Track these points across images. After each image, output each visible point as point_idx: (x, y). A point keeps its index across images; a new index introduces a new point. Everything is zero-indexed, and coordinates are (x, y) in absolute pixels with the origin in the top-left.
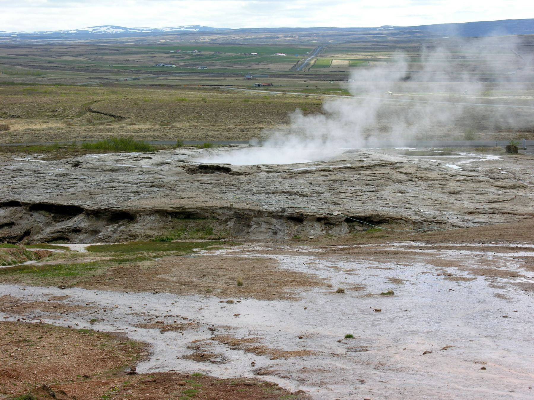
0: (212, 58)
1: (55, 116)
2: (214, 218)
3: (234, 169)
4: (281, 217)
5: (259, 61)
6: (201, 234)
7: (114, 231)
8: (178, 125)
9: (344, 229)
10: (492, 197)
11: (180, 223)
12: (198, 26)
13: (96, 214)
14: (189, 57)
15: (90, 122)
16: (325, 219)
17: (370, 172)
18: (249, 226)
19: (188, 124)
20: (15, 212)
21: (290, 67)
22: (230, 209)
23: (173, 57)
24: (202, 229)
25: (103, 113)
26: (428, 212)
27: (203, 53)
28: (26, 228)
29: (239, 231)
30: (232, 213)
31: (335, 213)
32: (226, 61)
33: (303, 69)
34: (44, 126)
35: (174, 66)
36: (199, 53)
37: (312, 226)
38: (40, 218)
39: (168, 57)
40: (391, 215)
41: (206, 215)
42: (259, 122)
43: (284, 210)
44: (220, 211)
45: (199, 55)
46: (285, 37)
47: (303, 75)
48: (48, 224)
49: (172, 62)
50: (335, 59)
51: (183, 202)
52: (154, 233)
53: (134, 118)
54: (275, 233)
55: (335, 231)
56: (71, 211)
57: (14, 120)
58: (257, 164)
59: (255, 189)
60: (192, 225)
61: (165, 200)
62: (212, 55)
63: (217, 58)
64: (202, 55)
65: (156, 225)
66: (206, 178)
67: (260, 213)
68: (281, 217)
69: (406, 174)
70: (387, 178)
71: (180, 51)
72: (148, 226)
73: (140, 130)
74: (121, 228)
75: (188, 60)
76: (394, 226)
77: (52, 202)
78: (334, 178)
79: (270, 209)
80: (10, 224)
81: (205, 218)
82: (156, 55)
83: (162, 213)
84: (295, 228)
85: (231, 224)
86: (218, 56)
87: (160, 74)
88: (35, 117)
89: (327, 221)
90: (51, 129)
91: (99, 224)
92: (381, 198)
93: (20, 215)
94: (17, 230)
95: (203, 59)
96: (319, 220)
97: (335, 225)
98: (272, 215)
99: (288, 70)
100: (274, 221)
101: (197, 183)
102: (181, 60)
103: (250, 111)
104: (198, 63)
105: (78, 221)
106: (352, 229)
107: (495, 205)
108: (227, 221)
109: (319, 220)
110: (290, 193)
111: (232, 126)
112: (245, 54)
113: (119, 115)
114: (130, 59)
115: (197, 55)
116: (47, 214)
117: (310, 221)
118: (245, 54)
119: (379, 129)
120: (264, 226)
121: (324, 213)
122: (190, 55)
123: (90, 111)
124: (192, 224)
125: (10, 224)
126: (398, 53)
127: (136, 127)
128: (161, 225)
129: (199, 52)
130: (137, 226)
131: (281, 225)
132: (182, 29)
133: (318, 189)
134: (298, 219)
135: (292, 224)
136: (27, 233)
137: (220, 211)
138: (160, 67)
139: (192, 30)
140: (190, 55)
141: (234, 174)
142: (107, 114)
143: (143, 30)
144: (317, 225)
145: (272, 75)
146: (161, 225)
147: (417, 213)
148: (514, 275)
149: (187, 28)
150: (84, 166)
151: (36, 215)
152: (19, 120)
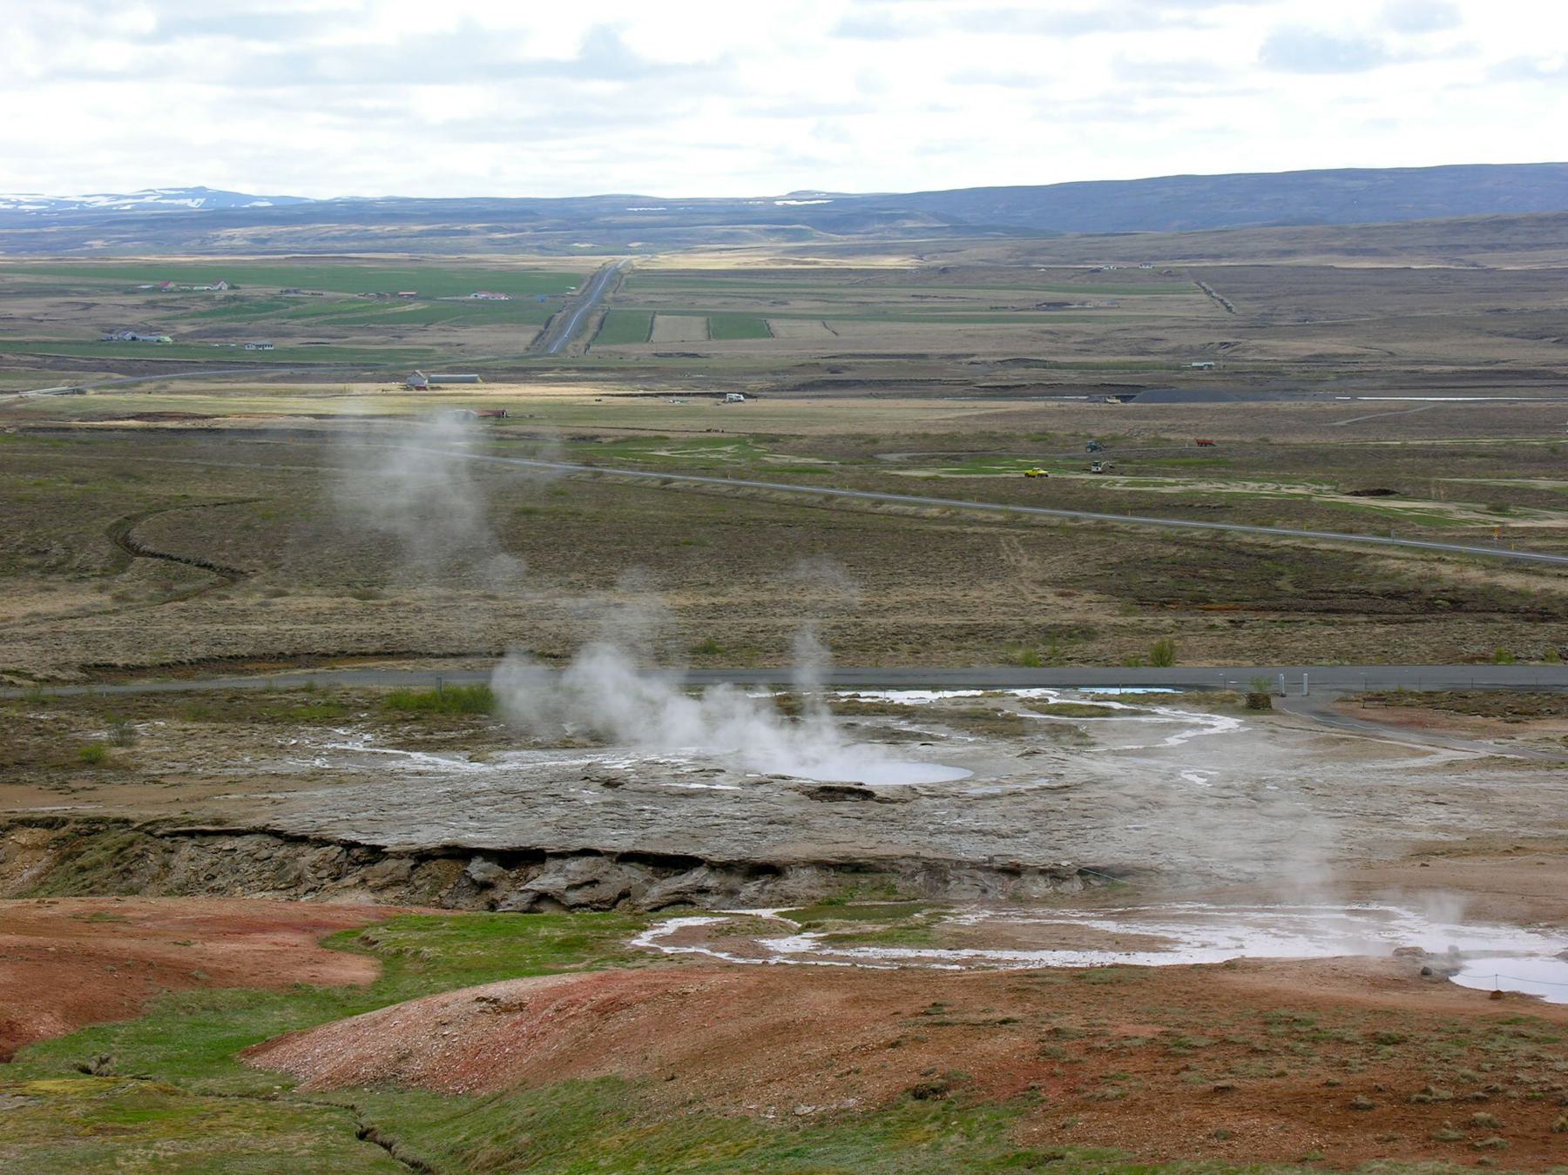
0: (278, 307)
2: (894, 871)
3: (880, 794)
4: (989, 869)
5: (427, 320)
6: (882, 894)
7: (761, 891)
9: (1077, 886)
11: (848, 880)
12: (203, 188)
13: (727, 867)
14: (204, 306)
16: (1051, 871)
18: (947, 882)
22: (916, 858)
23: (152, 305)
24: (881, 887)
25: (178, 559)
27: (247, 290)
29: (934, 889)
30: (919, 864)
31: (1064, 863)
32: (321, 319)
33: (569, 347)
35: (167, 339)
36: (232, 293)
38: (633, 875)
39: (137, 307)
40: (1137, 864)
41: (883, 867)
43: (991, 860)
44: (903, 862)
45: (235, 298)
46: (491, 230)
47: (578, 369)
48: (650, 882)
49: (153, 324)
50: (662, 313)
52: (820, 893)
54: (984, 891)
55: (1065, 887)
56: (685, 863)
58: (908, 783)
59: (931, 827)
60: (864, 881)
62: (276, 298)
63: (292, 308)
64: (242, 299)
65: (815, 881)
67: (960, 864)
68: (989, 869)
69: (1134, 797)
71: (172, 285)
72: (806, 883)
74: (768, 887)
75: (203, 314)
78: (1034, 807)
79: (970, 857)
80: (593, 883)
81: (880, 871)
82: (96, 300)
83: (822, 865)
84: (1013, 884)
85: (919, 879)
86: (296, 302)
87: (142, 372)
89: (1054, 874)
91: (734, 881)
92: (1113, 839)
93: (605, 869)
94: (606, 891)
95: (249, 311)
96: (1042, 872)
97: (1064, 879)
98: (975, 866)
99: (521, 349)
100: (980, 875)
102: (182, 317)
103: (563, 550)
104: (234, 325)
105: (696, 877)
106: (1086, 883)
107: (1270, 847)
108: (913, 875)
109: (1042, 872)
112: (379, 296)
113: (223, 563)
114: (16, 312)
115: (228, 299)
116: (642, 866)
117: (1030, 874)
118: (379, 296)
119: (1323, 885)
120: (968, 882)
121: (1050, 863)
122: (207, 298)
124: (864, 880)
125: (593, 883)
128: (823, 881)
129: (233, 288)
130: (790, 883)
131: (991, 879)
132: (149, 200)
133: (1019, 825)
134: (1014, 871)
135: (1006, 878)
136: (625, 895)
137: (903, 862)
138: (125, 344)
139: (182, 202)
140: (207, 298)
141: (882, 801)
142: (188, 562)
143: (19, 203)
144: (1040, 879)
146: (823, 881)
147: (1170, 861)
148: (1326, 933)
149: (165, 197)
151: (626, 868)
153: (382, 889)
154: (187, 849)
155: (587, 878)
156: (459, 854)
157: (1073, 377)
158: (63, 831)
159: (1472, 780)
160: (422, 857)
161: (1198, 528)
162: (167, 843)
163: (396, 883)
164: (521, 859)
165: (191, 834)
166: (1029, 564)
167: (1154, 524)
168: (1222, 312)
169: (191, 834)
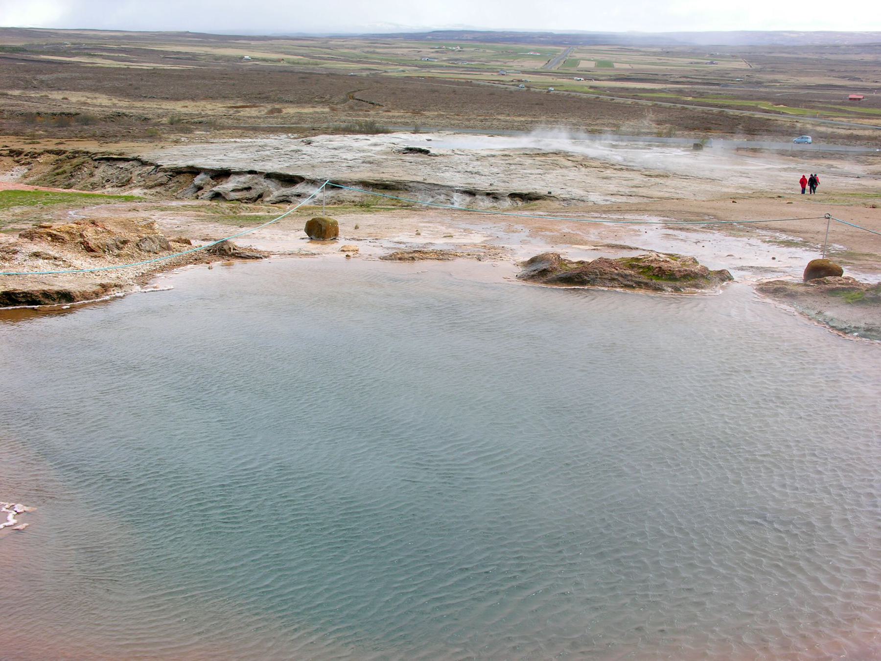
1: (322, 102)
8: (427, 113)
10: (635, 182)
11: (378, 193)
15: (351, 108)
16: (493, 194)
17: (543, 158)
19: (436, 113)
20: (253, 179)
21: (542, 65)
23: (437, 52)
26: (577, 192)
28: (260, 191)
34: (311, 110)
37: (482, 200)
42: (498, 114)
44: (411, 185)
51: (382, 175)
53: (390, 106)
57: (287, 105)
61: (371, 174)
66: (410, 157)
70: (556, 165)
73: (393, 117)
76: (548, 201)
77: (282, 172)
83: (365, 184)
88: (306, 102)
89: (494, 196)
90: (317, 113)
94: (253, 194)
101: (400, 162)
107: (634, 189)
109: (488, 194)
110: (471, 173)
111: (474, 116)
117: (481, 195)
123: (353, 98)
126: (142, 144)
127: (390, 114)
136: (260, 196)
145: (524, 72)
150: (314, 144)
151: (268, 181)
152: (290, 105)
153: (151, 187)
154: (103, 167)
155: (246, 186)
156: (194, 171)
157: (700, 81)
158: (62, 157)
159: (859, 550)
160: (177, 172)
161: (715, 110)
162: (96, 163)
163: (161, 184)
164: (222, 174)
165: (108, 159)
166: (651, 115)
167: (700, 108)
168: (749, 67)
169: (108, 159)
